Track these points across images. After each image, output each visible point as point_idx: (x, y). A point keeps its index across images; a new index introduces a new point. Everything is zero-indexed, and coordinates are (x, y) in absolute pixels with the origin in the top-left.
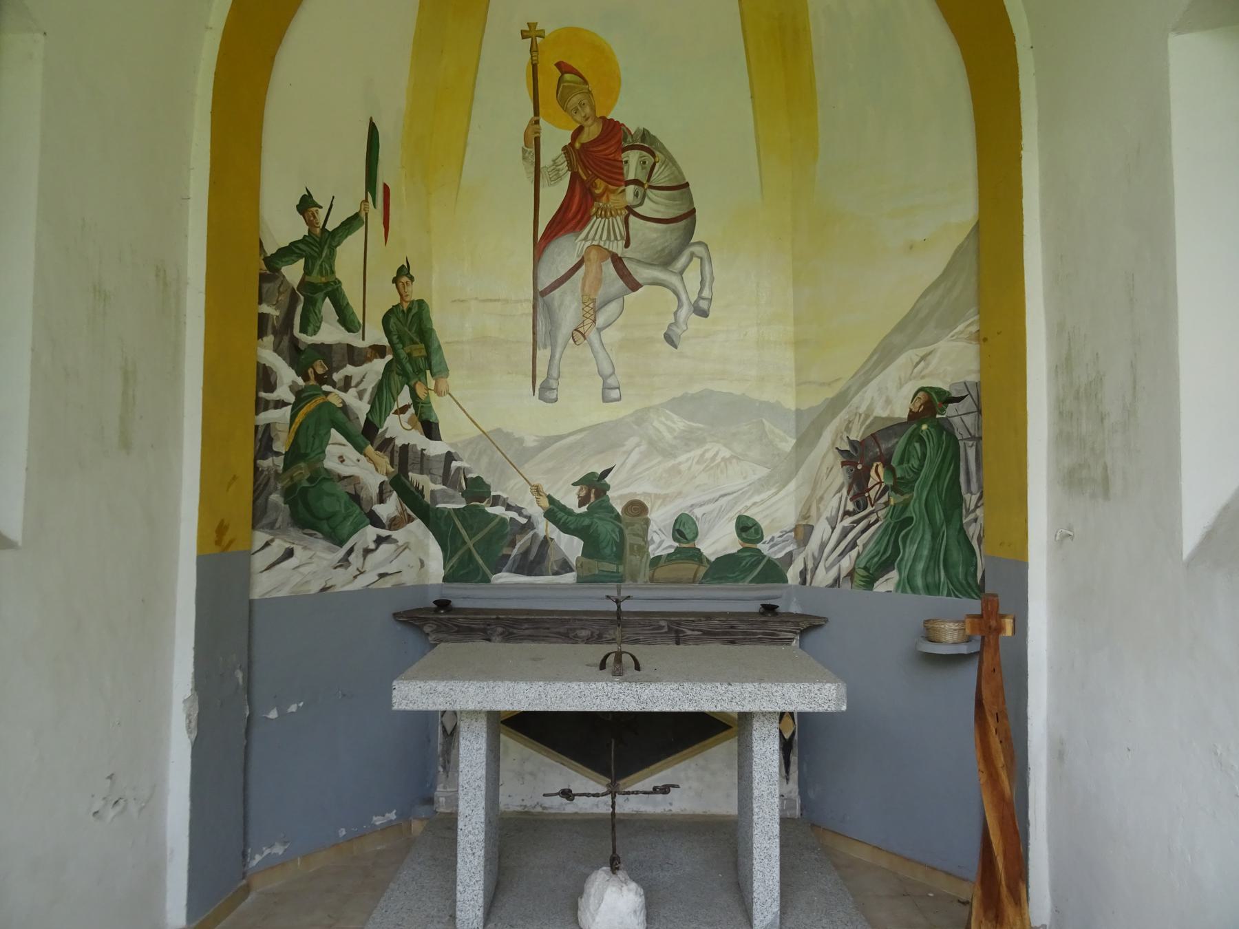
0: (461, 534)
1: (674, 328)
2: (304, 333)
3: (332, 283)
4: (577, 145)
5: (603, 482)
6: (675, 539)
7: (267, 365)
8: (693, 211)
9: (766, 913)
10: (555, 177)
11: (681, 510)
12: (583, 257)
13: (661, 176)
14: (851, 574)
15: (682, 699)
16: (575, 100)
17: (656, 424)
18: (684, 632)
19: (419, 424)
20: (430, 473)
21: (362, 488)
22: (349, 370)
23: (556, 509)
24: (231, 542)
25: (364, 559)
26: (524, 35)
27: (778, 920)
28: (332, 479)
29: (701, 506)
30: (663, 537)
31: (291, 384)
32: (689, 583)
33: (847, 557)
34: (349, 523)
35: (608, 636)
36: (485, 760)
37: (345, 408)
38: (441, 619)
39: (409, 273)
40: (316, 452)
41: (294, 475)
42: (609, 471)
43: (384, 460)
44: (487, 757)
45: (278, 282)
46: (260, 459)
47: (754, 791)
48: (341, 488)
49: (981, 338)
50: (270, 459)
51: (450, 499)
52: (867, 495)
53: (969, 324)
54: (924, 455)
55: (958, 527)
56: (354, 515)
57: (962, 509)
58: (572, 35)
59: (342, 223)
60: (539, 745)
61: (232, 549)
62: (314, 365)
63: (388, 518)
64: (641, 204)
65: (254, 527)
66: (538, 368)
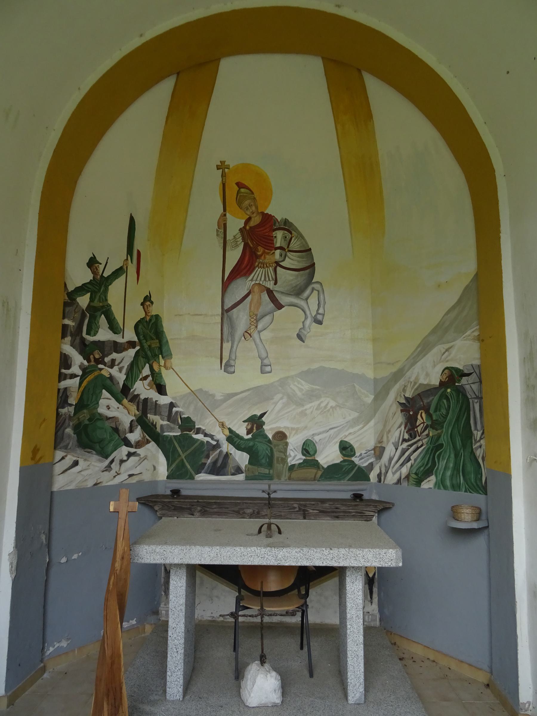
0: (177, 450)
1: (303, 331)
2: (89, 335)
3: (106, 306)
4: (248, 228)
5: (261, 420)
6: (303, 454)
7: (66, 354)
8: (314, 264)
9: (355, 692)
10: (235, 245)
11: (307, 437)
12: (250, 290)
13: (295, 245)
14: (408, 477)
15: (302, 558)
16: (247, 203)
17: (292, 386)
18: (308, 511)
19: (154, 386)
20: (160, 414)
21: (120, 424)
22: (114, 355)
23: (234, 436)
24: (41, 458)
25: (120, 466)
26: (218, 168)
27: (363, 697)
28: (102, 419)
29: (318, 435)
30: (296, 453)
31: (80, 364)
32: (312, 480)
33: (405, 466)
34: (112, 445)
35: (263, 513)
36: (185, 593)
37: (111, 378)
38: (164, 502)
39: (150, 300)
40: (93, 404)
41: (80, 417)
42: (265, 413)
43: (133, 408)
44: (186, 591)
45: (75, 306)
46: (60, 408)
47: (347, 615)
48: (107, 424)
49: (480, 339)
50: (67, 408)
51: (171, 430)
52: (416, 430)
53: (473, 331)
54: (449, 407)
55: (470, 450)
56: (115, 440)
57: (472, 439)
58: (246, 168)
59: (112, 273)
60: (222, 579)
61: (42, 462)
62: (94, 354)
63: (135, 441)
64: (283, 260)
65: (55, 448)
66: (224, 354)
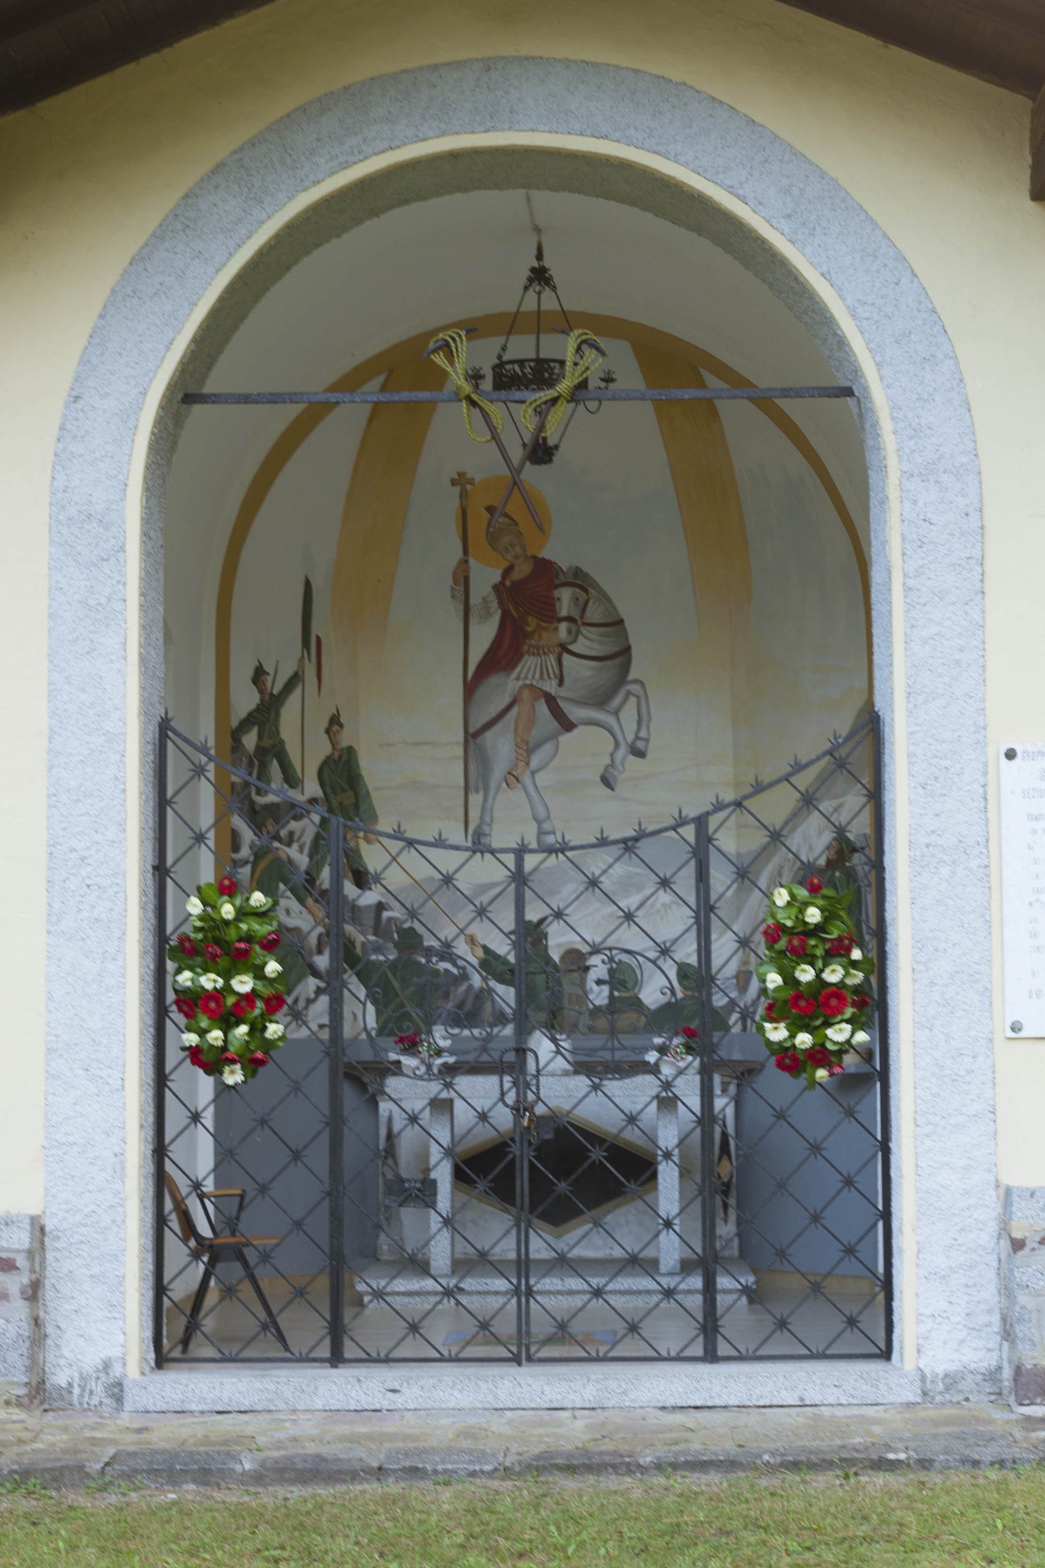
1: (611, 770)
13: (594, 612)
22: (293, 825)
26: (454, 483)
51: (378, 950)
64: (574, 641)
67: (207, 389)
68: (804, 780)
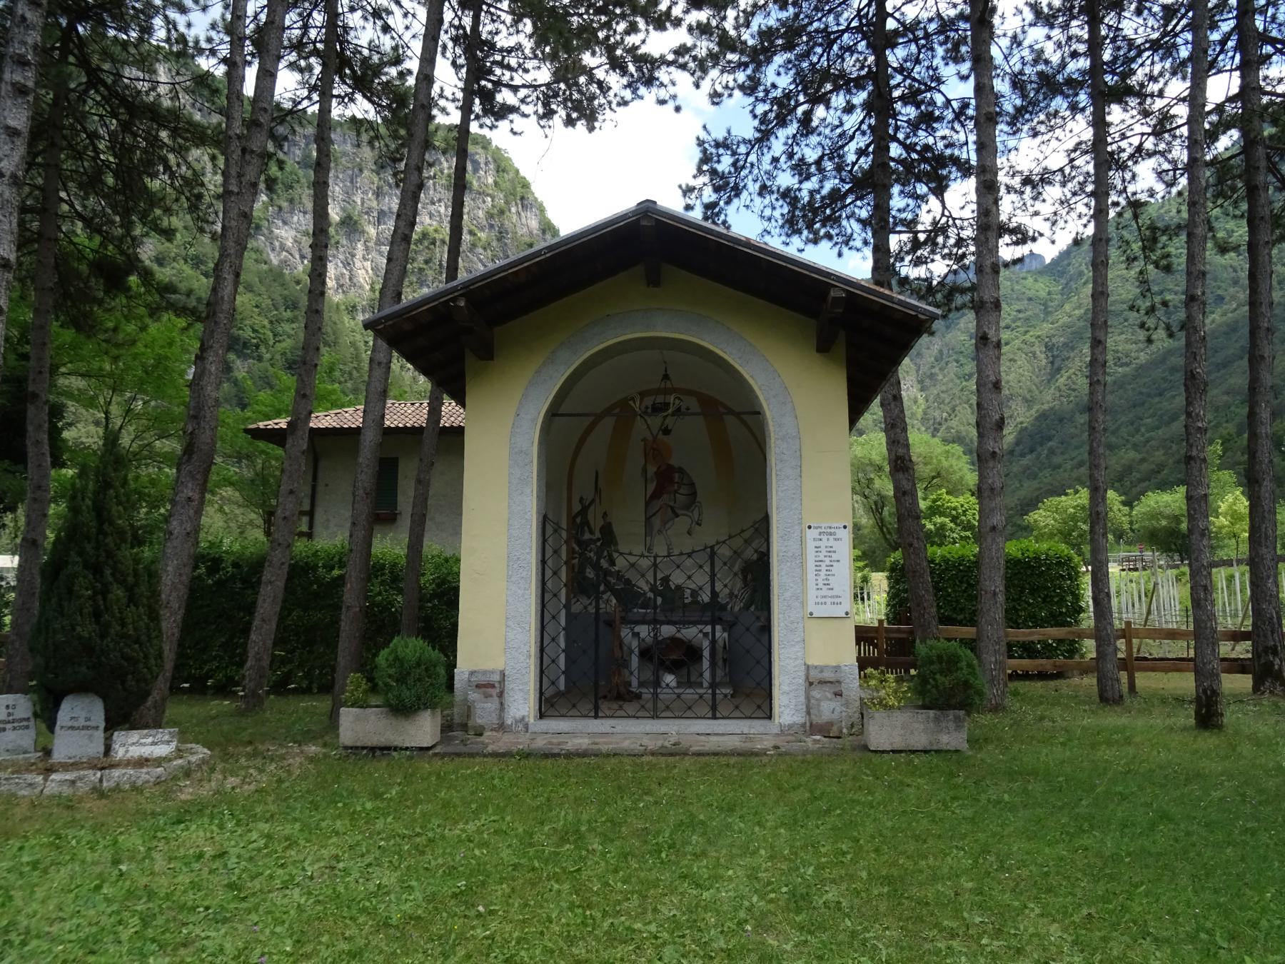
67: (560, 412)
68: (747, 535)
